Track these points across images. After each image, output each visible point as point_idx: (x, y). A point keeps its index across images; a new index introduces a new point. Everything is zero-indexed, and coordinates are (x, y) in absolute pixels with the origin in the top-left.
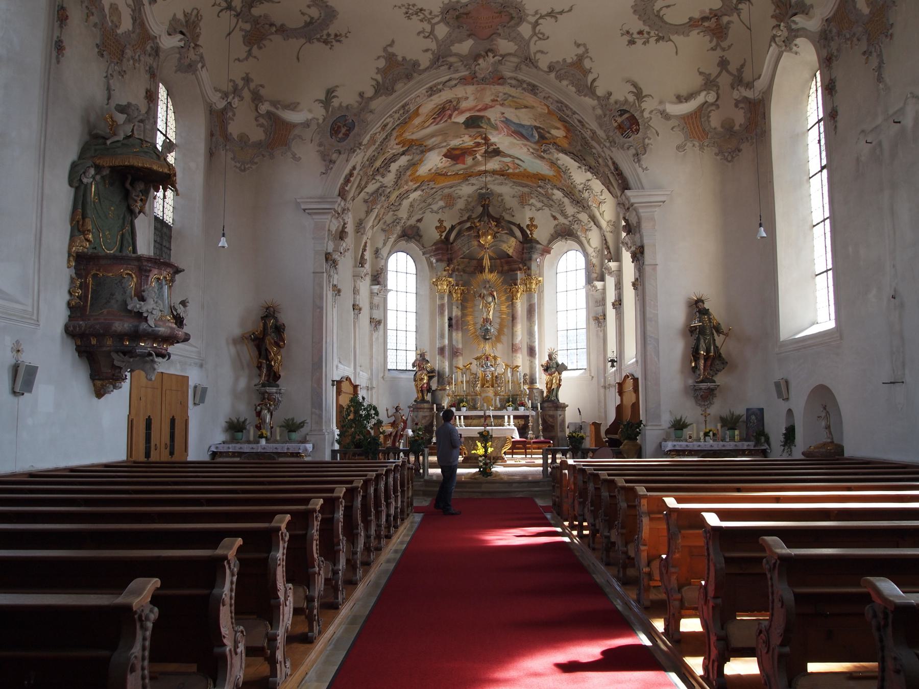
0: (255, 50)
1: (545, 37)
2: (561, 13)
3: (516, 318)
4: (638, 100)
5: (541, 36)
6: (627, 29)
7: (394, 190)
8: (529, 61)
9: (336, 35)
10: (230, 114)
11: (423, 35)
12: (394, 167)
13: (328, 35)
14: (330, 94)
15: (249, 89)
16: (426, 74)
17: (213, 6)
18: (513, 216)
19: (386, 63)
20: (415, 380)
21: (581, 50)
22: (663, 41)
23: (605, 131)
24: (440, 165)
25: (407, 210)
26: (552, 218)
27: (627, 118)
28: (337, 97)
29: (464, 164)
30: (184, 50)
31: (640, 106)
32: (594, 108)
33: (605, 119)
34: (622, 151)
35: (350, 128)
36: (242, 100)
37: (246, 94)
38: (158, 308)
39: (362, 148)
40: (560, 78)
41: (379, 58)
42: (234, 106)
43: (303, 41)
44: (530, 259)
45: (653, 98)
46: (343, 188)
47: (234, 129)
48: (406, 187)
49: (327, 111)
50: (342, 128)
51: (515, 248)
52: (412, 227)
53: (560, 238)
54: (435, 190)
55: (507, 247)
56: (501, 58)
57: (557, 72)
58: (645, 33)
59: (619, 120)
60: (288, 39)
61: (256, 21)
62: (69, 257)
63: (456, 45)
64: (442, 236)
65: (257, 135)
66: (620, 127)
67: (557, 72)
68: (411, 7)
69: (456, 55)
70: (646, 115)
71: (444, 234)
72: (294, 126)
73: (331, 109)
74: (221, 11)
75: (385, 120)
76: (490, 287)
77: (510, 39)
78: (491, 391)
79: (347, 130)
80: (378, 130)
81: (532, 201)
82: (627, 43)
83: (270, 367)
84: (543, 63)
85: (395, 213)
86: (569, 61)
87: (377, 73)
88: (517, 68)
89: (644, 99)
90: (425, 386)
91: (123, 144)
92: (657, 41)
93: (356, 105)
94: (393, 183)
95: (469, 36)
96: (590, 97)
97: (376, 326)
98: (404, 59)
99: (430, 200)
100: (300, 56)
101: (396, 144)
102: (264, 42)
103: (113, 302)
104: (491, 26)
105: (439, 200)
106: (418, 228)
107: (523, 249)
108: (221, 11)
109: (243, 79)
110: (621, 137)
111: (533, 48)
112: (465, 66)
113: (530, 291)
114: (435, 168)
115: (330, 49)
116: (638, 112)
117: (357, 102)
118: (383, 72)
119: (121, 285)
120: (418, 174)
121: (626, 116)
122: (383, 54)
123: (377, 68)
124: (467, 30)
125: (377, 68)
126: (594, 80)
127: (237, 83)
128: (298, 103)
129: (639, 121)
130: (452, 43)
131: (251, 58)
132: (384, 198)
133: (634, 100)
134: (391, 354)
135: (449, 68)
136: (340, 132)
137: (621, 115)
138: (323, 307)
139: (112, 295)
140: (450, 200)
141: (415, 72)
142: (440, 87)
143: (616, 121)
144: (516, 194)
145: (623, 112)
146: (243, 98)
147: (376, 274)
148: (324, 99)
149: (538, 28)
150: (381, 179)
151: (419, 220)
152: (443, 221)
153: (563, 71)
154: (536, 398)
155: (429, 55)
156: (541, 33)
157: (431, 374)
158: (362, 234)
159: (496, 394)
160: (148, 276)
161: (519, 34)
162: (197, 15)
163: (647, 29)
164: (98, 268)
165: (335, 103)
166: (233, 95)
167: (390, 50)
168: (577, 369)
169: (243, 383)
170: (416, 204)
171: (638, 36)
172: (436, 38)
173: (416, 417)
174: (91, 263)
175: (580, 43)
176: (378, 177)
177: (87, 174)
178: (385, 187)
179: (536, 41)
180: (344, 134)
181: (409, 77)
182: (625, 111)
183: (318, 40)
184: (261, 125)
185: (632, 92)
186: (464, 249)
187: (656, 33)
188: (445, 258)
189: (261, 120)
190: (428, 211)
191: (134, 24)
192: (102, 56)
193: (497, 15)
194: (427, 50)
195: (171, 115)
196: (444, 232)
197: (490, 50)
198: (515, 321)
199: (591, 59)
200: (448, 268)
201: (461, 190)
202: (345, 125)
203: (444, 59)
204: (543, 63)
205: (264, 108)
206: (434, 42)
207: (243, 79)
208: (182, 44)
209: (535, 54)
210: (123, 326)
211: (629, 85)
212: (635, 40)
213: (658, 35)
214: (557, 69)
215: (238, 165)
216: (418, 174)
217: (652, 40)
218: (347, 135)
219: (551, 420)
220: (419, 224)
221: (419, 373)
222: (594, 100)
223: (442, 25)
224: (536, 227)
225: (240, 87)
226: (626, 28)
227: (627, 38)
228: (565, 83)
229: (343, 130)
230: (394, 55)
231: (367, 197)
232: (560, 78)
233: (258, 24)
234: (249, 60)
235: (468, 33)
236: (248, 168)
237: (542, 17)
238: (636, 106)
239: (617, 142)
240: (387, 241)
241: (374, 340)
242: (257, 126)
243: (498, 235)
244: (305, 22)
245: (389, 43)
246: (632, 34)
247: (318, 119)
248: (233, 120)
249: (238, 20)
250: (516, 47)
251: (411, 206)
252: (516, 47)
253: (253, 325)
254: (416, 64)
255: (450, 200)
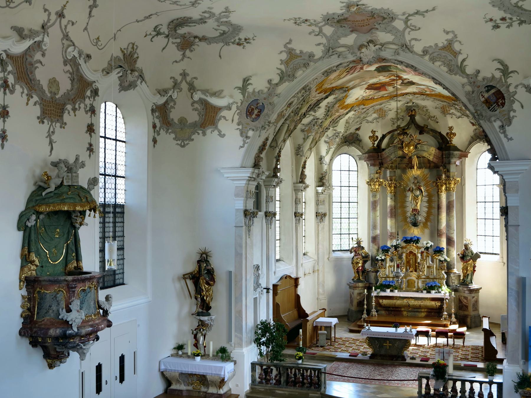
0: (188, 52)
1: (417, 28)
2: (427, 11)
3: (441, 208)
4: (504, 75)
5: (413, 28)
6: (490, 17)
7: (326, 119)
8: (406, 47)
9: (246, 39)
10: (172, 104)
11: (314, 34)
12: (324, 104)
13: (240, 39)
14: (246, 81)
15: (186, 81)
16: (320, 62)
17: (145, 36)
18: (437, 122)
19: (288, 56)
20: (352, 263)
21: (450, 36)
22: (525, 24)
23: (473, 105)
24: (365, 95)
25: (344, 126)
26: (471, 124)
27: (494, 93)
28: (251, 84)
29: (387, 91)
30: (122, 78)
31: (506, 82)
32: (463, 85)
33: (473, 95)
34: (489, 123)
35: (261, 110)
36: (181, 91)
37: (184, 86)
38: (80, 317)
39: (271, 125)
40: (433, 60)
41: (281, 52)
42: (174, 98)
43: (221, 44)
44: (449, 163)
45: (518, 73)
46: (259, 156)
47: (174, 115)
48: (337, 114)
49: (244, 97)
50: (255, 110)
51: (435, 155)
52: (352, 135)
53: (478, 140)
54: (365, 110)
55: (427, 155)
56: (381, 47)
57: (430, 55)
58: (507, 18)
59: (486, 95)
60: (210, 44)
61: (183, 36)
62: (20, 282)
63: (343, 39)
64: (374, 144)
65: (193, 117)
66: (487, 102)
67: (430, 55)
68: (297, 19)
69: (343, 46)
70: (512, 89)
71: (376, 143)
72: (220, 109)
73: (246, 95)
74: (153, 37)
75: (290, 99)
76: (418, 182)
77: (385, 30)
78: (415, 275)
79: (259, 112)
80: (284, 109)
81: (452, 111)
82: (492, 28)
83: (203, 300)
84: (418, 48)
85: (335, 128)
86: (441, 45)
87: (281, 64)
88: (397, 53)
89: (510, 75)
90: (360, 268)
91: (55, 194)
92: (520, 24)
93: (266, 90)
94: (324, 115)
95: (352, 31)
96: (460, 75)
97: (322, 218)
98: (301, 52)
99: (364, 115)
100: (221, 55)
101: (318, 94)
102: (193, 47)
103: (51, 311)
104: (369, 24)
105: (373, 113)
106: (358, 135)
107: (442, 155)
108: (153, 37)
109: (181, 74)
110: (488, 111)
111: (408, 38)
112: (352, 54)
113: (449, 190)
114: (361, 97)
115: (243, 48)
116: (504, 87)
117: (266, 87)
118: (286, 63)
119: (56, 299)
120: (346, 103)
121: (493, 91)
122: (284, 49)
123: (281, 60)
124: (350, 28)
125: (281, 60)
126: (464, 60)
127: (176, 78)
128: (222, 91)
129: (505, 95)
130: (339, 38)
131: (185, 59)
132: (317, 128)
133: (501, 76)
134: (336, 238)
135: (339, 57)
136: (253, 113)
137: (488, 91)
138: (242, 254)
139: (50, 306)
140: (382, 114)
141: (311, 62)
142: (335, 68)
143: (483, 97)
144: (438, 106)
145: (489, 88)
146: (182, 89)
147: (321, 176)
148: (242, 87)
149: (409, 23)
150: (313, 114)
151: (358, 129)
152: (375, 131)
153: (435, 54)
154: (453, 281)
155: (321, 47)
156: (412, 26)
157: (365, 258)
158: (301, 156)
159: (419, 277)
160: (74, 291)
161: (394, 27)
162: (133, 48)
163: (508, 16)
164: (40, 287)
165: (250, 89)
166: (173, 90)
167: (289, 46)
168: (493, 254)
169: (186, 310)
170: (351, 121)
171: (501, 22)
172: (325, 35)
173: (353, 293)
174: (36, 283)
175: (448, 30)
176: (312, 113)
177: (30, 220)
178: (317, 119)
179: (409, 32)
180: (256, 115)
181: (306, 65)
182: (492, 87)
183: (233, 43)
184: (196, 110)
185: (499, 69)
186: (391, 157)
187: (518, 18)
188: (378, 163)
189: (196, 105)
190: (364, 122)
191: (72, 84)
192: (43, 123)
193: (371, 18)
194: (319, 44)
195: (120, 120)
196: (376, 141)
197: (371, 41)
198: (440, 210)
199: (460, 42)
200: (379, 171)
201: (391, 105)
202: (257, 108)
203: (334, 50)
204: (418, 48)
205: (197, 96)
206: (324, 38)
207: (181, 74)
208: (121, 74)
209: (410, 41)
210: (56, 332)
211: (496, 62)
212: (499, 25)
213: (519, 20)
214: (431, 52)
215: (179, 142)
216: (346, 103)
217: (516, 24)
218: (258, 116)
219: (465, 301)
220: (357, 132)
221: (355, 258)
222: (463, 77)
223: (327, 27)
224: (455, 134)
225: (179, 81)
226: (488, 17)
227: (491, 24)
228: (438, 63)
229: (256, 112)
230: (293, 49)
231: (303, 128)
232: (433, 60)
233: (186, 37)
234: (184, 60)
235: (351, 29)
236: (187, 144)
237: (410, 15)
238: (502, 82)
239: (484, 115)
240: (329, 151)
241: (320, 229)
242: (193, 110)
243: (418, 146)
244: (220, 33)
245: (288, 41)
246: (496, 20)
247: (237, 103)
248: (175, 108)
249: (169, 39)
250: (393, 37)
251: (347, 122)
252: (393, 37)
253: (192, 267)
254: (311, 56)
255: (382, 114)
